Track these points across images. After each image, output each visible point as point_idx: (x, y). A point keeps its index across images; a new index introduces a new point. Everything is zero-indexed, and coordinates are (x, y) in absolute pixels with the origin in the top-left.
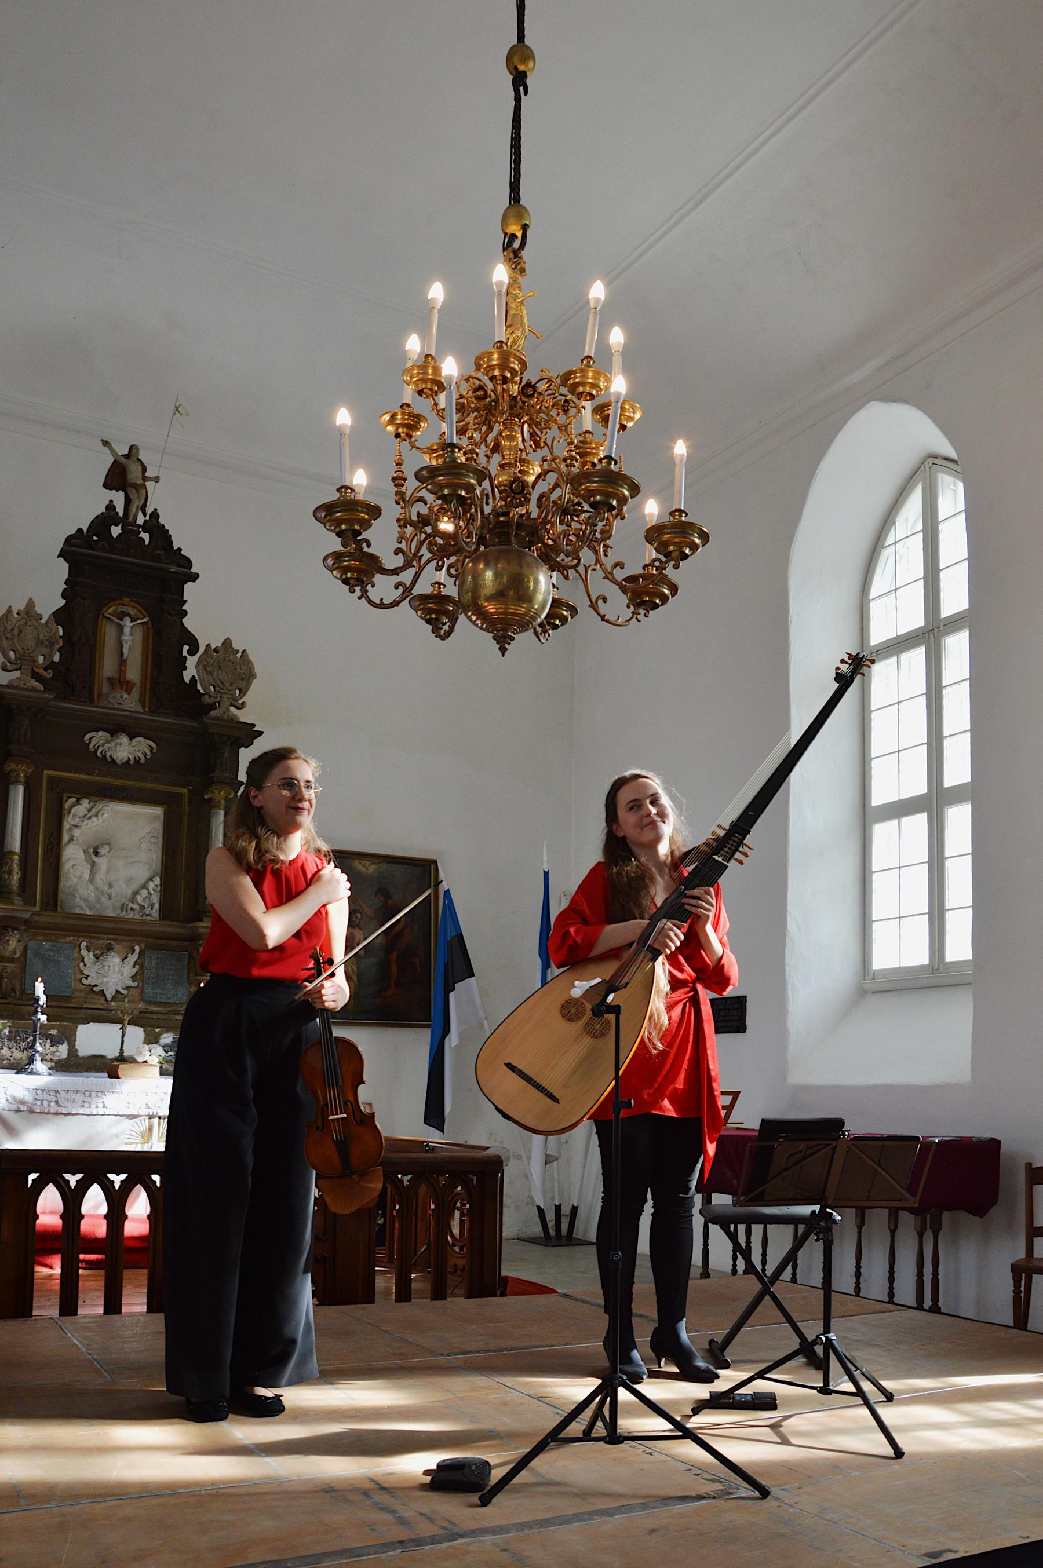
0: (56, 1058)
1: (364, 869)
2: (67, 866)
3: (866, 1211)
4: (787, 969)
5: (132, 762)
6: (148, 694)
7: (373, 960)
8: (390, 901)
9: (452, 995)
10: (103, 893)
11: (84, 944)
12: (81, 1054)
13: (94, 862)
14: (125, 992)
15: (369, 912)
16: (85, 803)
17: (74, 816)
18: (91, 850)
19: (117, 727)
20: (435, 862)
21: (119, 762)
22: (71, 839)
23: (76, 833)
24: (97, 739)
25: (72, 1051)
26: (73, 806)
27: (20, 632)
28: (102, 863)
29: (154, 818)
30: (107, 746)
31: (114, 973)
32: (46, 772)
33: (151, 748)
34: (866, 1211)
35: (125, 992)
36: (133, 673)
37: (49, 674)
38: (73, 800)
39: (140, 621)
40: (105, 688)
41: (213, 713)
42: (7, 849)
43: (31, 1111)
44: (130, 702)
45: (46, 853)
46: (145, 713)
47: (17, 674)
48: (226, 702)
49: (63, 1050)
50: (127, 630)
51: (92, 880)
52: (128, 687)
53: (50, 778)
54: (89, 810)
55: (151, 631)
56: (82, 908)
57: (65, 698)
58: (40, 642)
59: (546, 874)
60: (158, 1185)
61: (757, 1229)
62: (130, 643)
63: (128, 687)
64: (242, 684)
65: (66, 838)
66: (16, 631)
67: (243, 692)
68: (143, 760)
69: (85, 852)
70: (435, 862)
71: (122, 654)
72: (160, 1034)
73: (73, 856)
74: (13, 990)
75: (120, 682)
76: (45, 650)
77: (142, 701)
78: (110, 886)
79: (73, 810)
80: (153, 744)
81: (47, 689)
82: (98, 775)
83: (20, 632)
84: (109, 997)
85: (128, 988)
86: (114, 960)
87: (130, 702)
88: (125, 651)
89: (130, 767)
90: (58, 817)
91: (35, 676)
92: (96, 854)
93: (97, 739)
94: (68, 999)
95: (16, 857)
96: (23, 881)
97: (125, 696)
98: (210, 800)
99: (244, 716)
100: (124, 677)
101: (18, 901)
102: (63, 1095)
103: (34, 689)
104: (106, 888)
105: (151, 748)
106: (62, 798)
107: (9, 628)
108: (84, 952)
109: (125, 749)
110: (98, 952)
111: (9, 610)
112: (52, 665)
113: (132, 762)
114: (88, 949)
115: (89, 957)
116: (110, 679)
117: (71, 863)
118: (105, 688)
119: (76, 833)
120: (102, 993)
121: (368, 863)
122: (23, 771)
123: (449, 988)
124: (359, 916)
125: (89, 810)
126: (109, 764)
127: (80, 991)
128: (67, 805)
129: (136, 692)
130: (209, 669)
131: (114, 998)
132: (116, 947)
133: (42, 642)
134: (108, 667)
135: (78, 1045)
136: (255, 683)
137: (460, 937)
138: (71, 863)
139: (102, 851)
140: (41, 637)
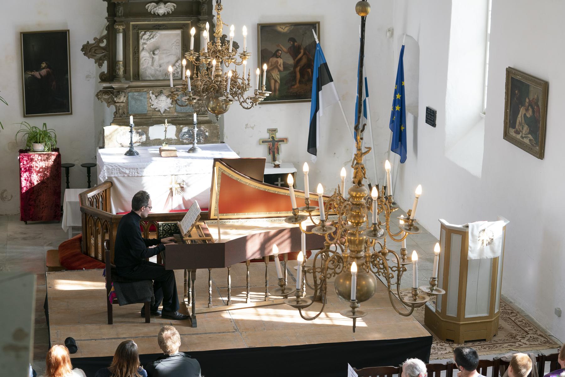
0: (141, 141)
1: (282, 30)
2: (142, 61)
4: (446, 106)
7: (288, 72)
8: (296, 44)
9: (320, 92)
11: (151, 92)
12: (151, 139)
13: (153, 58)
14: (168, 110)
16: (148, 33)
20: (319, 23)
21: (161, 15)
22: (143, 49)
23: (145, 46)
25: (148, 138)
26: (143, 35)
29: (178, 35)
31: (163, 103)
32: (131, 23)
33: (174, 6)
35: (168, 110)
38: (143, 32)
42: (117, 59)
43: (128, 176)
49: (144, 138)
51: (152, 65)
53: (133, 25)
56: (149, 77)
59: (403, 47)
60: (150, 247)
61: (246, 295)
65: (141, 48)
68: (171, 12)
70: (319, 23)
72: (182, 128)
73: (144, 55)
74: (124, 113)
78: (160, 66)
80: (175, 5)
84: (162, 112)
85: (169, 108)
86: (163, 98)
90: (137, 39)
92: (154, 54)
94: (145, 115)
95: (121, 63)
96: (125, 71)
101: (123, 80)
102: (139, 170)
106: (138, 34)
108: (151, 95)
110: (157, 94)
114: (153, 94)
115: (153, 97)
120: (159, 111)
122: (121, 28)
123: (319, 89)
124: (280, 52)
127: (150, 111)
128: (141, 35)
131: (164, 112)
132: (164, 91)
135: (150, 135)
137: (325, 65)
139: (156, 52)
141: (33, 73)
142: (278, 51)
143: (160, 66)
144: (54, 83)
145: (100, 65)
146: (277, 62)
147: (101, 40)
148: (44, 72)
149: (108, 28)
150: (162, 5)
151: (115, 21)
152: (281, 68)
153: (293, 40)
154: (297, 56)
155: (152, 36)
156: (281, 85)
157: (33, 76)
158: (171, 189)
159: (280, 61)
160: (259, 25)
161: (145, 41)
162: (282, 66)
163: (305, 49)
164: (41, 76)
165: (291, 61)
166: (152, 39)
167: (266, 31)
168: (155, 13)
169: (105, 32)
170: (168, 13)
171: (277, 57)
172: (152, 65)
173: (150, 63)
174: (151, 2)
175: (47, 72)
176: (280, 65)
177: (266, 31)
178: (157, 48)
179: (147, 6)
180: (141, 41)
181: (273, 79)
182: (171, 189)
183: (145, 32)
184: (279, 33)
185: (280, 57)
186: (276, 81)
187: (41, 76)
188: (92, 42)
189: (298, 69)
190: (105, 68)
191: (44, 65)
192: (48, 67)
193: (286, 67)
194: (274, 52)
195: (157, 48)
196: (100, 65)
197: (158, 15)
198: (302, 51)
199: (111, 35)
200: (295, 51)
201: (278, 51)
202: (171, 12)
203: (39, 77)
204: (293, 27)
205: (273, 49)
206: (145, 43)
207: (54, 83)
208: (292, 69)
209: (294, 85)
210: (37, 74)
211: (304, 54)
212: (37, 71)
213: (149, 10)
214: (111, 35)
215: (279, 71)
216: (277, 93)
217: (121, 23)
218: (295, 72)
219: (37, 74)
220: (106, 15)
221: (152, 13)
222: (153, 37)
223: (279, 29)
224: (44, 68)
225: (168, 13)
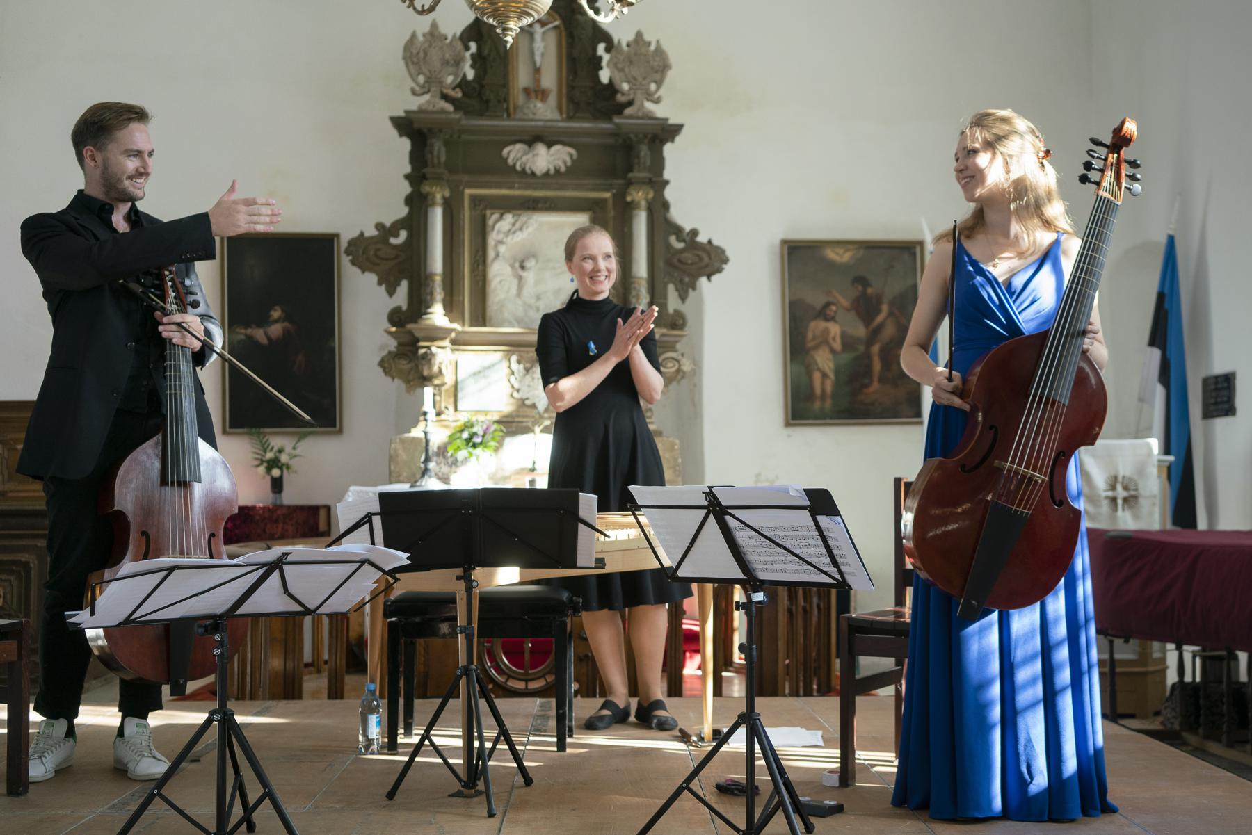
3: (743, 800)
5: (552, 172)
6: (564, 101)
8: (870, 291)
10: (530, 306)
15: (845, 302)
16: (509, 218)
17: (499, 232)
18: (517, 265)
19: (533, 139)
23: (502, 249)
24: (515, 153)
27: (426, 54)
28: (529, 276)
30: (524, 158)
32: (468, 192)
34: (743, 800)
36: (549, 80)
37: (458, 94)
38: (496, 216)
39: (551, 26)
40: (521, 99)
41: (627, 111)
44: (546, 112)
45: (473, 270)
46: (563, 121)
47: (427, 97)
48: (639, 97)
50: (538, 37)
51: (519, 294)
52: (542, 94)
54: (514, 225)
55: (564, 34)
57: (481, 115)
58: (445, 63)
62: (541, 50)
63: (542, 94)
64: (657, 76)
65: (491, 254)
66: (421, 54)
67: (659, 84)
68: (563, 169)
69: (512, 266)
71: (534, 63)
75: (536, 92)
76: (451, 69)
77: (560, 108)
78: (538, 298)
79: (497, 226)
80: (573, 151)
81: (457, 108)
82: (519, 188)
83: (426, 54)
87: (546, 112)
88: (538, 59)
89: (550, 178)
90: (481, 232)
91: (445, 97)
92: (523, 267)
93: (515, 153)
97: (539, 105)
98: (632, 202)
99: (659, 111)
100: (539, 85)
103: (443, 111)
104: (533, 301)
105: (571, 156)
107: (415, 52)
109: (544, 159)
110: (528, 365)
111: (414, 35)
112: (463, 84)
113: (552, 172)
116: (527, 91)
117: (498, 279)
118: (521, 99)
119: (502, 249)
120: (534, 406)
121: (841, 251)
124: (834, 308)
125: (514, 225)
126: (527, 176)
128: (490, 222)
129: (552, 99)
130: (620, 66)
133: (447, 62)
134: (522, 78)
136: (671, 75)
138: (498, 279)
139: (530, 264)
140: (447, 56)
141: (249, 331)
142: (828, 304)
143: (538, 298)
144: (300, 358)
145: (391, 292)
146: (827, 331)
147: (394, 229)
148: (276, 330)
149: (409, 200)
150: (541, 149)
151: (424, 177)
152: (837, 345)
153: (861, 281)
154: (873, 319)
155: (518, 225)
156: (837, 384)
157: (250, 338)
158: (456, 409)
159: (835, 329)
160: (784, 242)
161: (501, 237)
162: (838, 340)
163: (892, 304)
164: (269, 338)
165: (860, 331)
166: (519, 233)
167: (800, 257)
168: (524, 170)
169: (403, 211)
170: (557, 171)
171: (828, 319)
172: (519, 294)
173: (514, 291)
174: (514, 142)
175: (284, 329)
176: (834, 339)
177: (800, 257)
178: (532, 255)
179: (505, 151)
180: (492, 239)
181: (819, 370)
182: (456, 409)
183: (502, 215)
184: (831, 265)
185: (833, 319)
186: (824, 375)
187: (269, 338)
188: (371, 232)
189: (876, 349)
190: (401, 297)
191: (276, 313)
192: (287, 317)
193: (848, 343)
194: (819, 306)
195: (532, 255)
196: (391, 292)
197: (533, 174)
198: (885, 308)
199: (415, 222)
200: (866, 308)
201: (828, 304)
202: (563, 169)
203: (264, 341)
204: (862, 252)
205: (816, 298)
206: (501, 242)
207: (300, 358)
208: (862, 348)
209: (866, 386)
210: (259, 334)
211: (891, 314)
212: (259, 325)
213: (510, 162)
214: (415, 222)
215: (833, 351)
216: (828, 404)
217: (438, 179)
218: (868, 356)
219: (259, 334)
220: (408, 169)
221: (518, 168)
222: (521, 229)
223: (830, 254)
224: (276, 321)
225: (557, 171)
